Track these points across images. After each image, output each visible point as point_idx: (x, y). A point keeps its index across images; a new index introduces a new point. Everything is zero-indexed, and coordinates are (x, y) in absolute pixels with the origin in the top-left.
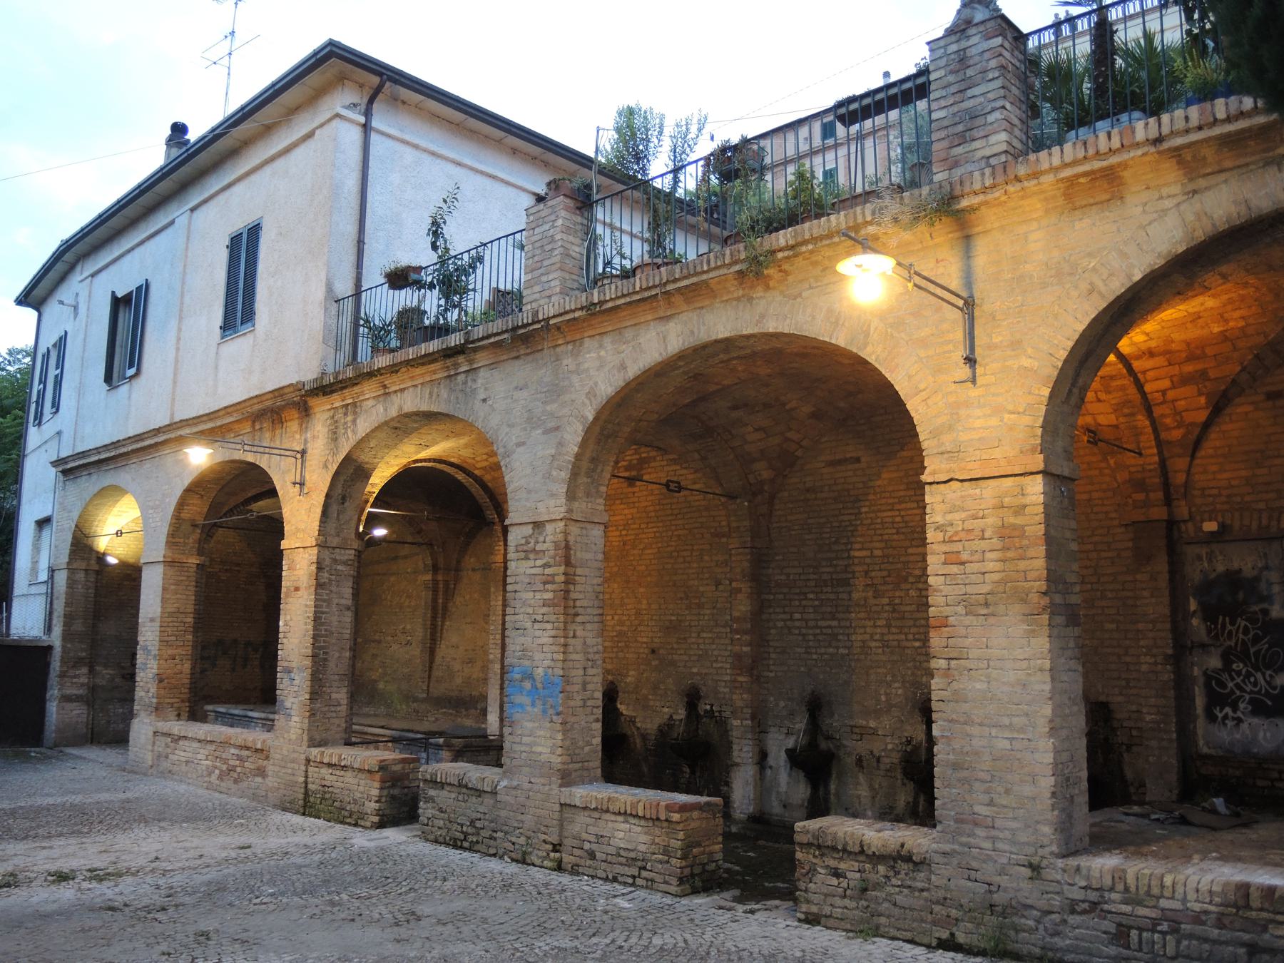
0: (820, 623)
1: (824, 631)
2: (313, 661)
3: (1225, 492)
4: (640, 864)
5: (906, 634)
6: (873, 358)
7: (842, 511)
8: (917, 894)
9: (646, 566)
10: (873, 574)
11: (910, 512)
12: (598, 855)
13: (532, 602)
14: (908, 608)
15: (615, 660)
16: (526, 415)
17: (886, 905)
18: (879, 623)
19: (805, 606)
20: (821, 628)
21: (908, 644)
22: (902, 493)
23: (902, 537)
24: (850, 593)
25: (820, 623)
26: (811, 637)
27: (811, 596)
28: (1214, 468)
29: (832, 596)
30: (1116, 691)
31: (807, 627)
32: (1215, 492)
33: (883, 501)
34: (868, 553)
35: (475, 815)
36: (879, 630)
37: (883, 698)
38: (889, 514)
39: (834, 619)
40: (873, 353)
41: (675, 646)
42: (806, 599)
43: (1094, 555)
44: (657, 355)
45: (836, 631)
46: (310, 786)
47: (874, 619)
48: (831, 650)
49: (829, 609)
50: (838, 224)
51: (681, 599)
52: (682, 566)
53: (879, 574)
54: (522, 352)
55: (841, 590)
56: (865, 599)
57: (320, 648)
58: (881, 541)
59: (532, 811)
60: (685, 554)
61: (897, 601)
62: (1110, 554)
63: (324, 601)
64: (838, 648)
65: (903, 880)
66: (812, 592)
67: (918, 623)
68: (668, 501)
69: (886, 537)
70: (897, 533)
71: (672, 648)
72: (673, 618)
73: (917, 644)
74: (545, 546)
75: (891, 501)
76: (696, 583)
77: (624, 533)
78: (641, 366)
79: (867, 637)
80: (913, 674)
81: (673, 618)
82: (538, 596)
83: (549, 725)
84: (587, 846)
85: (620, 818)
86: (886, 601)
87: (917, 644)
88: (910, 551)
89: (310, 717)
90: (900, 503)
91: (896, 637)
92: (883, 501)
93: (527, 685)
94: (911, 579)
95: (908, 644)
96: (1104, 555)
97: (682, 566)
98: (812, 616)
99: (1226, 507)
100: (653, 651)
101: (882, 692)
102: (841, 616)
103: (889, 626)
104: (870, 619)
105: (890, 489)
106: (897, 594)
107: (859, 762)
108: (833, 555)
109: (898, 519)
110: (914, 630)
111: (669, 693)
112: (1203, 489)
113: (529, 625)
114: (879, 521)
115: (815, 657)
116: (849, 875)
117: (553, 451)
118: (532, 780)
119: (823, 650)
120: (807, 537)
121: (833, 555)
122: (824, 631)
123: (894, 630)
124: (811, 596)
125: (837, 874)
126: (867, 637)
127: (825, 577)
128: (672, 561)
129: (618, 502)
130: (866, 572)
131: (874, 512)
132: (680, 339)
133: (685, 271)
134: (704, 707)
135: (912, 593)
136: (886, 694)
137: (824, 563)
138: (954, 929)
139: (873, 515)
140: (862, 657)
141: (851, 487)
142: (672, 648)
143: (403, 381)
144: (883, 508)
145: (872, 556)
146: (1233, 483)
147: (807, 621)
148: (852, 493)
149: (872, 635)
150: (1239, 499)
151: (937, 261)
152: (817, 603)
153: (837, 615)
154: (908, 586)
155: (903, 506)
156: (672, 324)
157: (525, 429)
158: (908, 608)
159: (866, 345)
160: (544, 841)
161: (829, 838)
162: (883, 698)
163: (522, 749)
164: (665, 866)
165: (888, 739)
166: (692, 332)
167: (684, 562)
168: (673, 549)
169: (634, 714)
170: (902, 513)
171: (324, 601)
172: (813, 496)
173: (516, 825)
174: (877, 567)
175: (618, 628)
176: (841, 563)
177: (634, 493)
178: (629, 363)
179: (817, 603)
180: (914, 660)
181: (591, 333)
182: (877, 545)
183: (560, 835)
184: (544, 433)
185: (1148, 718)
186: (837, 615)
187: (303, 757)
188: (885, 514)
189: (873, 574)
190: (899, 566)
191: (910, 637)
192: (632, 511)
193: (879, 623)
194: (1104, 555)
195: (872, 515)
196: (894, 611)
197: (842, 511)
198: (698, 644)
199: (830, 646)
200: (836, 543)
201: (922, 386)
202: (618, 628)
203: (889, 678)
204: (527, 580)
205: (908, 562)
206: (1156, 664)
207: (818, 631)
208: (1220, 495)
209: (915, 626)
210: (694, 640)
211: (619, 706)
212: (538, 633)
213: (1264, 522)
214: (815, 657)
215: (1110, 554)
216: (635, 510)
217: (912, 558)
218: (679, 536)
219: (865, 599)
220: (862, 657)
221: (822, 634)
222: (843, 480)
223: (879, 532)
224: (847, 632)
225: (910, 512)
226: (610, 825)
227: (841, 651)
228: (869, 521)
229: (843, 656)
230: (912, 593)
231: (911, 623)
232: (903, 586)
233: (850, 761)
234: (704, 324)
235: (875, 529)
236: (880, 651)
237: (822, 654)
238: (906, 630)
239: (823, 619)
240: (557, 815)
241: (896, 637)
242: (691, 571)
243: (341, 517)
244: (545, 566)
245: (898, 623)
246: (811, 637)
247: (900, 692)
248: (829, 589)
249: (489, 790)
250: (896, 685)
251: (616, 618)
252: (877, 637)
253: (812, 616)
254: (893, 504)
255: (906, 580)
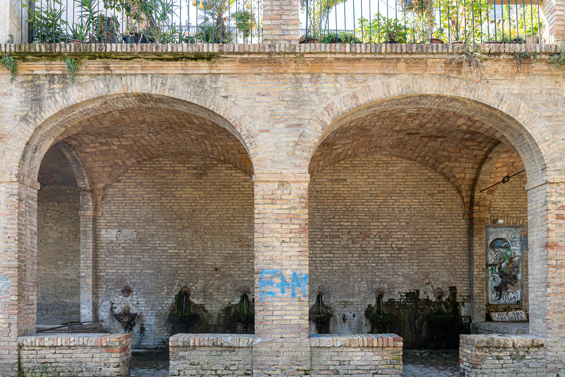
0: (323, 255)
1: (325, 259)
2: (19, 271)
3: (502, 210)
4: (373, 372)
5: (368, 260)
6: (522, 121)
7: (337, 204)
8: (539, 361)
9: (211, 223)
10: (352, 233)
11: (372, 207)
12: (341, 371)
13: (280, 230)
14: (369, 249)
15: (187, 275)
16: (269, 113)
17: (524, 368)
18: (355, 255)
19: (314, 248)
20: (324, 257)
21: (369, 265)
22: (368, 198)
23: (368, 217)
24: (340, 241)
25: (323, 255)
26: (318, 262)
27: (318, 242)
28: (498, 200)
29: (330, 243)
30: (459, 282)
31: (316, 257)
32: (498, 209)
33: (358, 201)
34: (350, 223)
35: (228, 363)
36: (355, 259)
37: (357, 288)
38: (362, 206)
39: (331, 253)
40: (522, 118)
41: (232, 266)
42: (315, 244)
43: (453, 230)
44: (382, 95)
45: (332, 259)
46: (24, 365)
47: (352, 254)
48: (329, 268)
49: (328, 249)
50: (521, 49)
51: (236, 242)
52: (237, 225)
53: (355, 233)
54: (263, 71)
55: (335, 240)
56: (348, 245)
57: (22, 261)
58: (357, 218)
59: (285, 354)
60: (239, 218)
61: (364, 246)
62: (459, 230)
63: (23, 225)
64: (333, 267)
65: (532, 356)
66: (319, 241)
67: (374, 255)
68: (227, 189)
69: (360, 217)
70: (365, 216)
71: (230, 268)
72: (230, 252)
73: (374, 265)
74: (290, 197)
75: (363, 201)
76: (246, 234)
77: (193, 204)
78: (370, 99)
79: (349, 261)
80: (371, 277)
81: (230, 252)
82: (285, 227)
83: (297, 303)
84: (332, 368)
85: (359, 349)
86: (358, 245)
87: (374, 265)
88: (371, 224)
89: (18, 313)
90: (367, 202)
91: (363, 262)
92: (358, 201)
93: (278, 280)
94: (371, 236)
95: (369, 265)
96: (456, 230)
97: (237, 225)
98: (319, 252)
99: (502, 215)
100: (216, 269)
101: (356, 286)
102: (335, 252)
103: (360, 257)
104: (350, 254)
105: (363, 195)
106: (364, 242)
107: (344, 319)
108: (331, 224)
109: (366, 209)
110: (372, 259)
111: (228, 291)
112: (494, 208)
113: (277, 244)
114: (356, 209)
115: (320, 271)
116: (504, 358)
117: (296, 139)
118: (283, 336)
119: (325, 268)
120: (316, 214)
121: (331, 224)
122: (325, 259)
123: (362, 258)
124: (318, 242)
125: (498, 358)
126: (349, 261)
127: (326, 234)
128: (230, 222)
129: (188, 187)
130: (349, 232)
131: (353, 205)
132: (400, 89)
133: (419, 49)
134: (385, 299)
135: (372, 242)
136: (358, 287)
137: (326, 227)
138: (559, 373)
139: (353, 207)
140: (346, 271)
141: (341, 192)
142: (230, 268)
143: (132, 68)
144: (359, 204)
145: (352, 225)
146: (505, 206)
147: (315, 254)
148: (342, 195)
149: (351, 261)
150: (506, 212)
151: (556, 82)
152: (321, 246)
153: (332, 252)
154: (370, 239)
155: (369, 204)
156: (393, 79)
157: (269, 122)
158: (369, 249)
159: (518, 114)
160: (298, 370)
161: (496, 342)
162: (357, 288)
163: (274, 318)
164: (392, 370)
165: (359, 306)
166: (409, 87)
167: (238, 223)
168: (230, 215)
169: (203, 303)
170: (368, 207)
171: (23, 225)
172: (321, 195)
173: (272, 363)
174: (355, 230)
175: (189, 257)
176: (335, 227)
177: (201, 183)
178: (360, 96)
179: (321, 246)
180: (372, 271)
181: (328, 71)
182: (355, 220)
183: (311, 365)
184: (287, 127)
185: (476, 292)
186: (332, 252)
187: (15, 344)
188: (360, 206)
189: (352, 233)
190: (366, 230)
191: (371, 261)
192: (199, 193)
193: (355, 255)
194: (456, 230)
195: (352, 206)
196: (362, 250)
197: (337, 204)
198: (248, 265)
199: (329, 266)
200: (333, 217)
201: (547, 139)
202: (189, 257)
203: (359, 280)
204: (275, 217)
205: (370, 229)
206: (479, 271)
207: (322, 259)
208: (500, 210)
209: (373, 257)
210: (245, 263)
211: (191, 299)
212: (285, 249)
213: (515, 221)
214: (320, 271)
215: (459, 230)
216: (202, 192)
217: (372, 227)
218: (234, 209)
219: (348, 245)
220: (346, 271)
221: (324, 260)
222: (337, 189)
223: (356, 214)
224: (338, 259)
225: (372, 207)
226: (350, 354)
227: (335, 268)
228: (351, 209)
229: (336, 270)
230: (372, 242)
231: (371, 255)
232: (367, 239)
233: (339, 318)
234: (416, 84)
235: (354, 213)
236: (355, 268)
237: (324, 270)
238: (369, 259)
239: (325, 253)
240: (309, 354)
241: (363, 262)
242: (243, 228)
243: (32, 163)
244: (290, 209)
245: (364, 256)
246: (318, 262)
247: (365, 285)
248: (329, 240)
249: (245, 345)
250: (363, 283)
251: (188, 251)
252: (354, 262)
253: (319, 252)
254: (363, 202)
255: (369, 237)
